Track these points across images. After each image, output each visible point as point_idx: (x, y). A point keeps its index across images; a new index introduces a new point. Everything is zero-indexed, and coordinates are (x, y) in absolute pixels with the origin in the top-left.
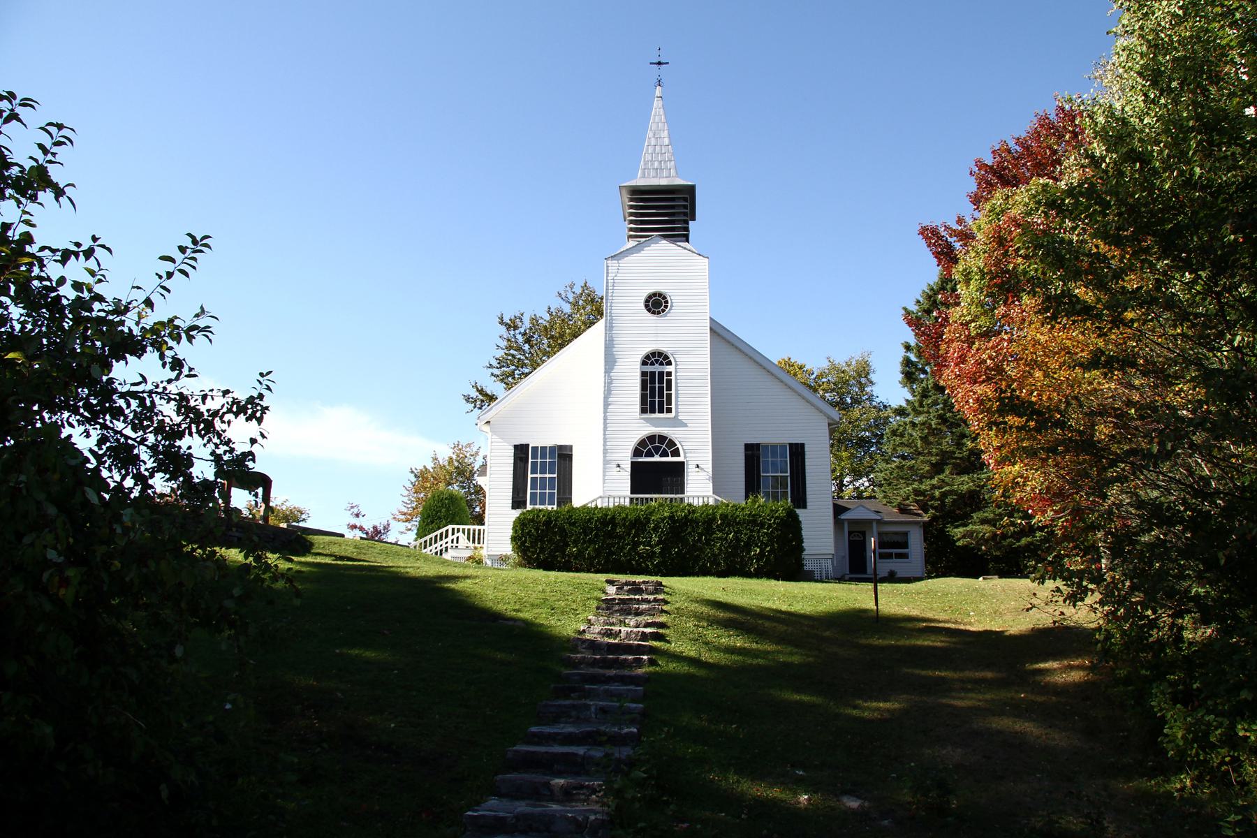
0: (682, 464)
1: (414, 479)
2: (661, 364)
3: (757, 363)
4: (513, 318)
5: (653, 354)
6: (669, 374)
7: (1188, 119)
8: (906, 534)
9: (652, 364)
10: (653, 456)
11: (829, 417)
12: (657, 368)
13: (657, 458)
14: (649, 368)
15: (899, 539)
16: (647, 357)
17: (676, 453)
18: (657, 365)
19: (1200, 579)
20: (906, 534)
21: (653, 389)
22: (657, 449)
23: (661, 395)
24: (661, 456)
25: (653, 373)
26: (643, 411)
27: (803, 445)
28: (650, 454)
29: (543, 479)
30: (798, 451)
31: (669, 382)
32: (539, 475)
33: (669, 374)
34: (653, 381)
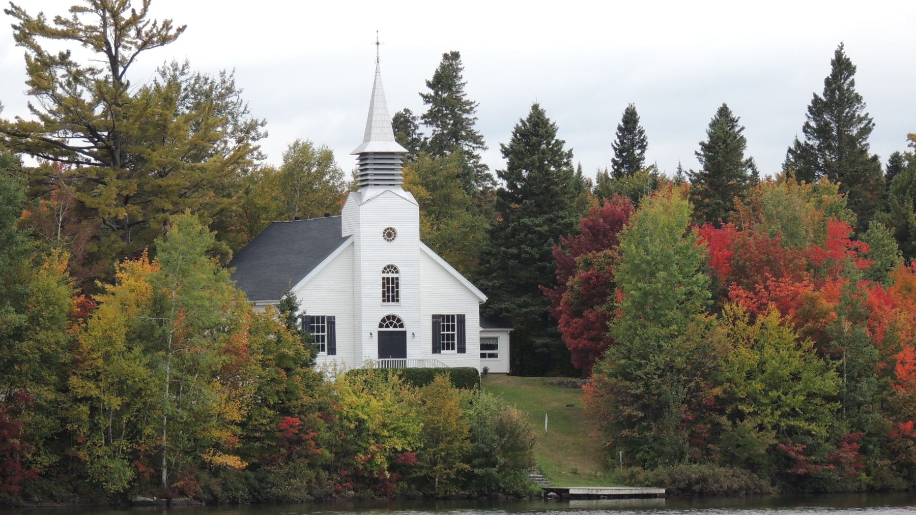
0: (405, 332)
1: (477, 135)
2: (393, 272)
3: (445, 270)
4: (869, 117)
5: (388, 317)
6: (397, 279)
7: (834, 106)
8: (496, 339)
9: (388, 272)
10: (389, 327)
11: (479, 298)
12: (390, 275)
13: (391, 329)
14: (386, 275)
15: (492, 342)
16: (383, 320)
17: (402, 326)
18: (390, 273)
19: (718, 405)
20: (496, 339)
21: (388, 288)
22: (391, 323)
23: (388, 288)
24: (394, 327)
25: (388, 279)
26: (384, 301)
27: (464, 316)
28: (387, 326)
29: (318, 332)
30: (462, 319)
31: (397, 284)
32: (321, 334)
33: (397, 279)
34: (388, 283)
